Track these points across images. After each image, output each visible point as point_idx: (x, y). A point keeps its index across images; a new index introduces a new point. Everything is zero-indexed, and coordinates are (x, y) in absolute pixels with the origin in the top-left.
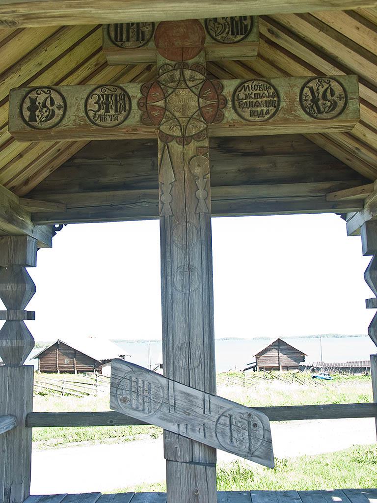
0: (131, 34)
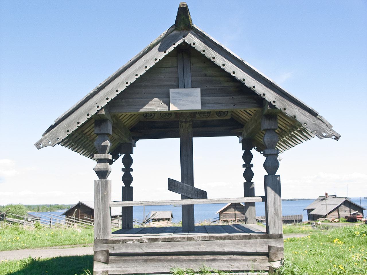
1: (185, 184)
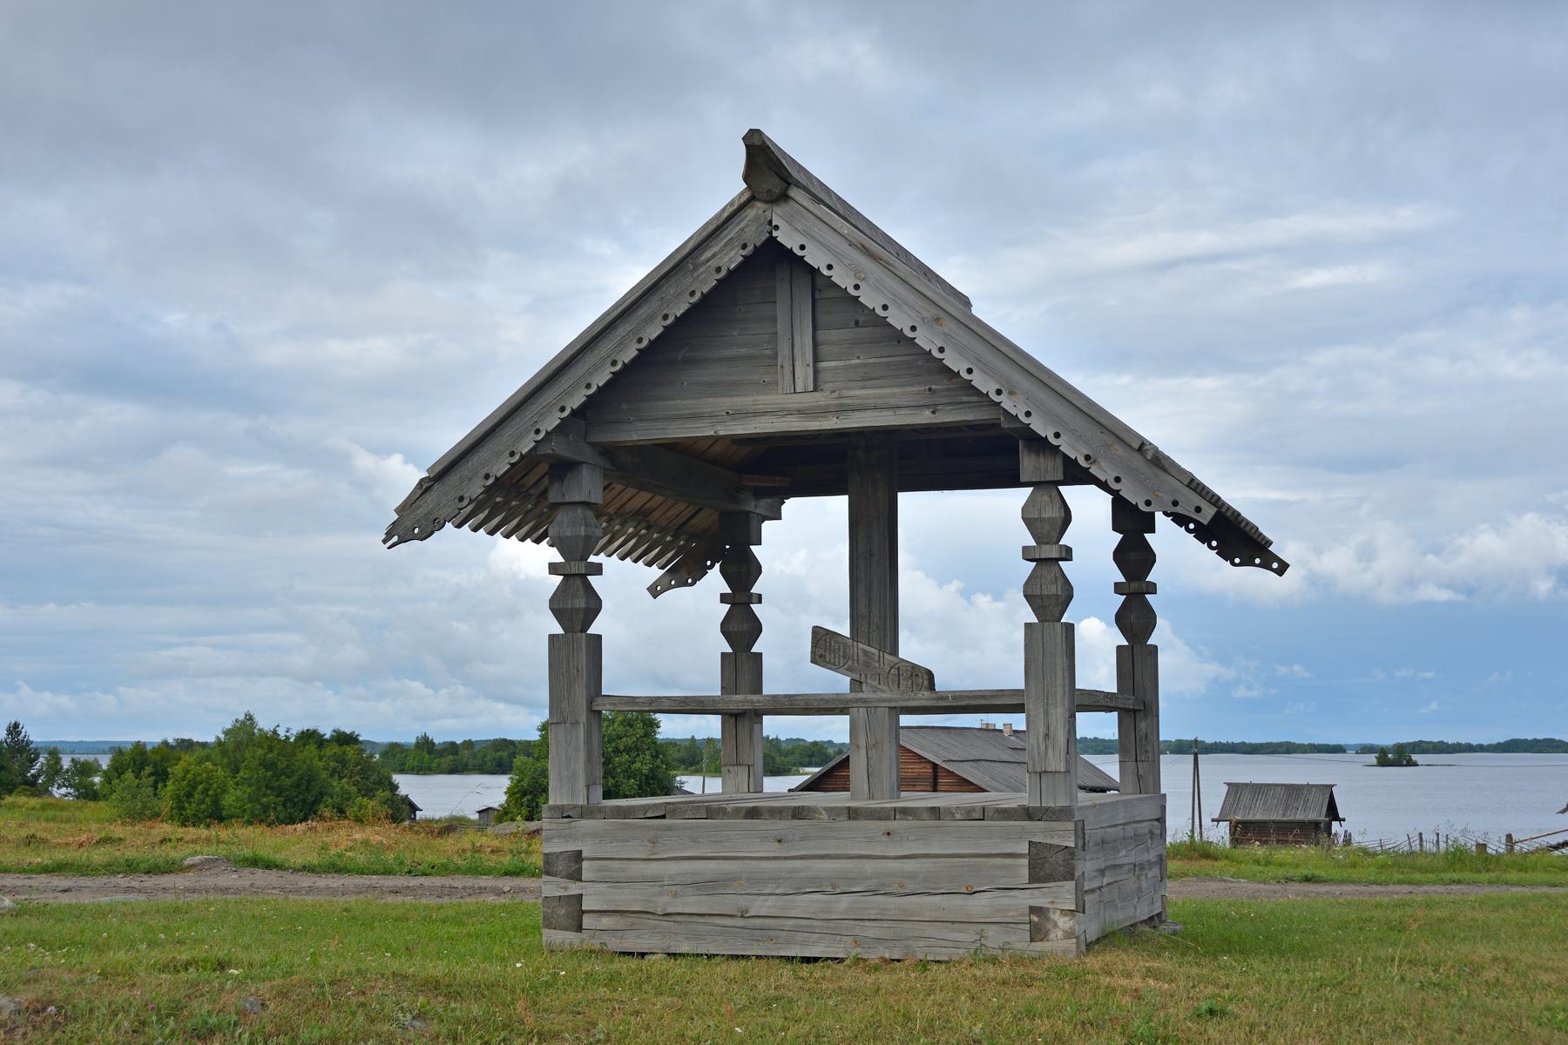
1: (861, 645)
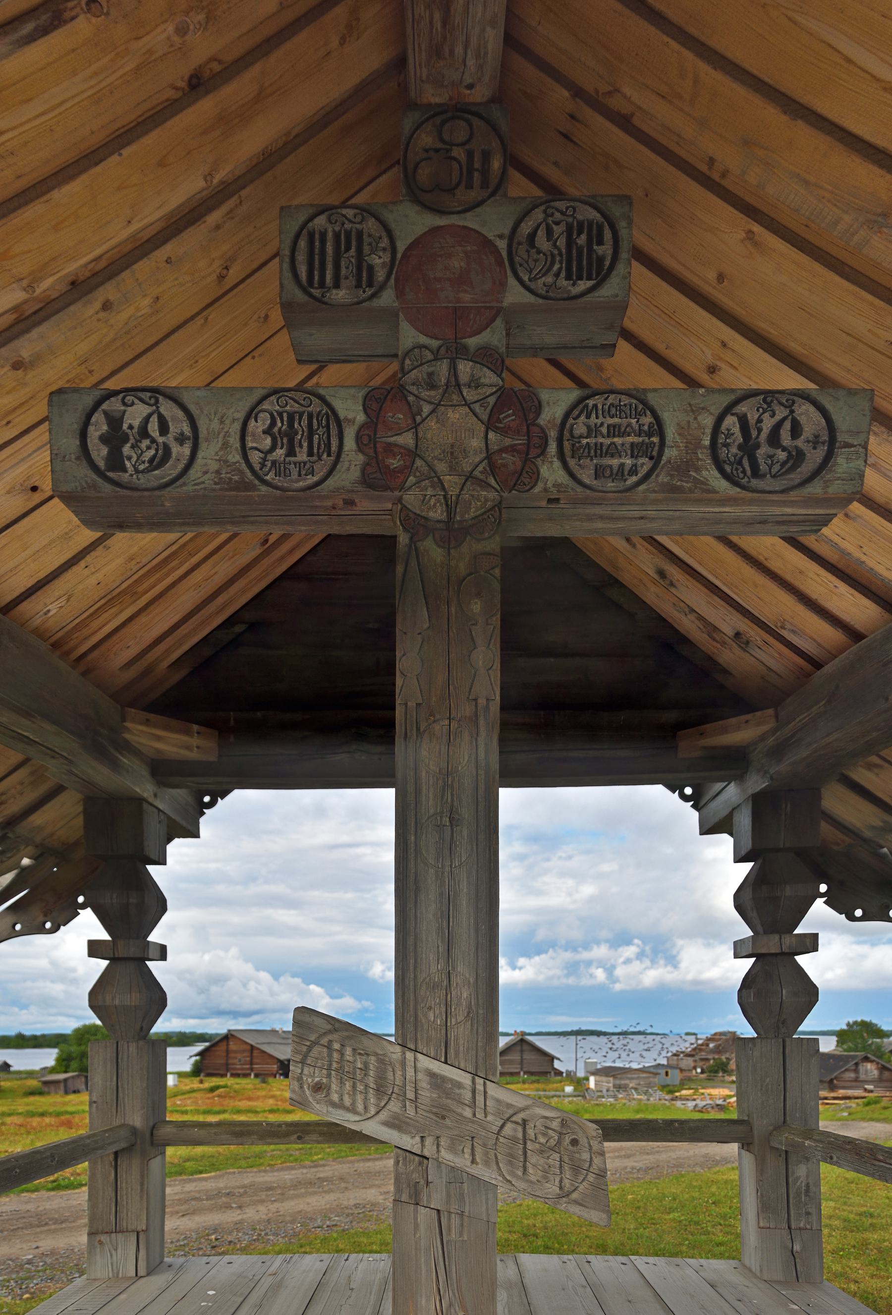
0: (343, 271)
1: (425, 1062)
